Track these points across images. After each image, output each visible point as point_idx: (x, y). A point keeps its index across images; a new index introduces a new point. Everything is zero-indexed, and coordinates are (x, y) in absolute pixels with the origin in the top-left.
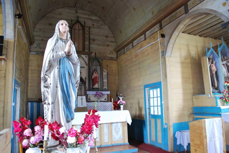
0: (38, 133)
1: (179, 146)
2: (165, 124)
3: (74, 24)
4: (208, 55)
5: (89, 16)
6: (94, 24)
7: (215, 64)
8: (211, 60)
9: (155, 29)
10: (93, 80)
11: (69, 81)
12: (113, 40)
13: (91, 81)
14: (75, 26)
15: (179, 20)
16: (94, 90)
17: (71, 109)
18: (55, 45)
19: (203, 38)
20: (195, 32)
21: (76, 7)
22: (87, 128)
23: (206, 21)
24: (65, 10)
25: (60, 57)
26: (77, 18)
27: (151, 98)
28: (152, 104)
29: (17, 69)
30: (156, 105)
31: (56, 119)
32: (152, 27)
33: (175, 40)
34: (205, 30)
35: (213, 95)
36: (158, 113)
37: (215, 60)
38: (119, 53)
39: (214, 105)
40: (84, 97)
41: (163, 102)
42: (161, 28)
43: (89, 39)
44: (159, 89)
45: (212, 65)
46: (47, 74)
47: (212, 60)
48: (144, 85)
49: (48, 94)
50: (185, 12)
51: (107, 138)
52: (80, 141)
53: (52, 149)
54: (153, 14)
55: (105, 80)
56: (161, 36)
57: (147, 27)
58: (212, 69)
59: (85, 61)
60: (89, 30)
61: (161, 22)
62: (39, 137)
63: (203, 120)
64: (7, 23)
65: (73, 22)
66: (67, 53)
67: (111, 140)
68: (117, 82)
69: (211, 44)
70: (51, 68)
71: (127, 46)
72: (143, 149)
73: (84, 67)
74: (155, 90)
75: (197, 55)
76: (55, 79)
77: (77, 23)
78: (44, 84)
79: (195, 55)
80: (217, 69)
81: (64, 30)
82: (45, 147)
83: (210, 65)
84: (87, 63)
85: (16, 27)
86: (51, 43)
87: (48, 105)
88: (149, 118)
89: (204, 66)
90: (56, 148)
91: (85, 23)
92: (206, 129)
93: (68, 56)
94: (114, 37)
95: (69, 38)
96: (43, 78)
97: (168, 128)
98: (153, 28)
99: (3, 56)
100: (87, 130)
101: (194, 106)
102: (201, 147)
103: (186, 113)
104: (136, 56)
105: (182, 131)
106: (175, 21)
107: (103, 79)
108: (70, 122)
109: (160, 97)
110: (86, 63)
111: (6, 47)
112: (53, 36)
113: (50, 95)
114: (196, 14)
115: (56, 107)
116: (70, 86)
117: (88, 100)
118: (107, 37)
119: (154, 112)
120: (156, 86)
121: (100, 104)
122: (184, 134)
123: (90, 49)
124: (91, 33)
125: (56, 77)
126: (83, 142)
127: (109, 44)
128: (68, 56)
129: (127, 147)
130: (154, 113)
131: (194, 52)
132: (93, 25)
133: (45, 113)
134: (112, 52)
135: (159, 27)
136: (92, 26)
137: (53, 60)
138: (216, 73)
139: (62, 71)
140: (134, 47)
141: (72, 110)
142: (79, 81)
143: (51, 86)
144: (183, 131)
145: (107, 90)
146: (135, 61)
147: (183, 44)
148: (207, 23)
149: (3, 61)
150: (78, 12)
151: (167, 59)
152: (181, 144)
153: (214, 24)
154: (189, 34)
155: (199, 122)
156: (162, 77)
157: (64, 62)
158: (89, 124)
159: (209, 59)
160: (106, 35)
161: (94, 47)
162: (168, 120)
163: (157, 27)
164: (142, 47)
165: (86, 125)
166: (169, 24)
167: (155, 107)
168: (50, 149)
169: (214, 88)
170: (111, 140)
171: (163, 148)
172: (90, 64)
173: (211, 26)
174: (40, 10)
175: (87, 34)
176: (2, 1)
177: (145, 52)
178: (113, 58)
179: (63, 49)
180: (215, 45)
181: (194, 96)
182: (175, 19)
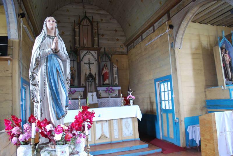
1: (191, 141)
2: (177, 118)
3: (82, 20)
4: (220, 44)
5: (97, 11)
7: (229, 54)
8: (224, 50)
9: (163, 20)
10: (103, 76)
11: (58, 78)
12: (123, 34)
13: (101, 77)
14: (83, 21)
15: (187, 8)
16: (105, 86)
17: (60, 106)
18: (41, 43)
19: (215, 26)
21: (83, 2)
22: (78, 126)
23: (216, 8)
24: (72, 7)
25: (47, 54)
27: (162, 92)
28: (163, 99)
29: (24, 68)
30: (167, 99)
31: (45, 116)
33: (184, 31)
36: (169, 107)
37: (228, 50)
38: (129, 47)
39: (229, 98)
40: (95, 94)
41: (173, 96)
42: (169, 18)
43: (98, 35)
44: (169, 83)
45: (225, 54)
47: (226, 50)
48: (155, 78)
51: (117, 134)
53: (43, 146)
55: (116, 76)
56: (169, 27)
58: (225, 59)
59: (94, 57)
60: (97, 25)
61: (169, 12)
62: (28, 135)
63: (213, 113)
65: (81, 18)
68: (128, 77)
71: (136, 39)
72: (154, 145)
73: (93, 63)
74: (166, 84)
75: (209, 45)
76: (43, 77)
77: (85, 19)
78: (32, 82)
80: (231, 59)
81: (51, 27)
82: (33, 145)
83: (223, 55)
84: (97, 59)
85: (20, 27)
86: (38, 40)
87: (37, 103)
89: (216, 56)
90: (48, 145)
91: (93, 18)
93: (56, 53)
95: (57, 34)
96: (30, 76)
99: (9, 56)
100: (76, 126)
101: (207, 99)
102: (211, 142)
103: (199, 106)
104: (146, 49)
105: (194, 125)
106: (183, 10)
107: (113, 74)
109: (161, 92)
110: (95, 59)
113: (39, 93)
115: (45, 104)
117: (99, 97)
118: (116, 31)
119: (165, 106)
120: (166, 79)
121: (111, 100)
122: (196, 128)
123: (100, 44)
124: (99, 28)
125: (44, 75)
127: (119, 38)
128: (56, 53)
129: (138, 143)
130: (165, 108)
131: (205, 42)
133: (35, 111)
135: (167, 18)
136: (100, 21)
137: (40, 57)
138: (230, 63)
139: (49, 68)
140: (143, 40)
143: (39, 83)
144: (196, 125)
145: (118, 86)
147: (193, 34)
150: (86, 7)
152: (193, 139)
153: (226, 11)
154: (199, 23)
155: (209, 116)
156: (172, 70)
157: (52, 59)
159: (222, 49)
160: (115, 30)
161: (103, 42)
162: (179, 115)
163: (165, 18)
164: (151, 39)
165: (76, 122)
166: (177, 14)
167: (166, 101)
168: (41, 147)
169: (228, 79)
171: (175, 144)
172: (100, 59)
173: (223, 13)
174: (47, 8)
175: (96, 30)
176: (4, 2)
177: (154, 44)
179: (50, 46)
181: (206, 88)
182: (183, 8)
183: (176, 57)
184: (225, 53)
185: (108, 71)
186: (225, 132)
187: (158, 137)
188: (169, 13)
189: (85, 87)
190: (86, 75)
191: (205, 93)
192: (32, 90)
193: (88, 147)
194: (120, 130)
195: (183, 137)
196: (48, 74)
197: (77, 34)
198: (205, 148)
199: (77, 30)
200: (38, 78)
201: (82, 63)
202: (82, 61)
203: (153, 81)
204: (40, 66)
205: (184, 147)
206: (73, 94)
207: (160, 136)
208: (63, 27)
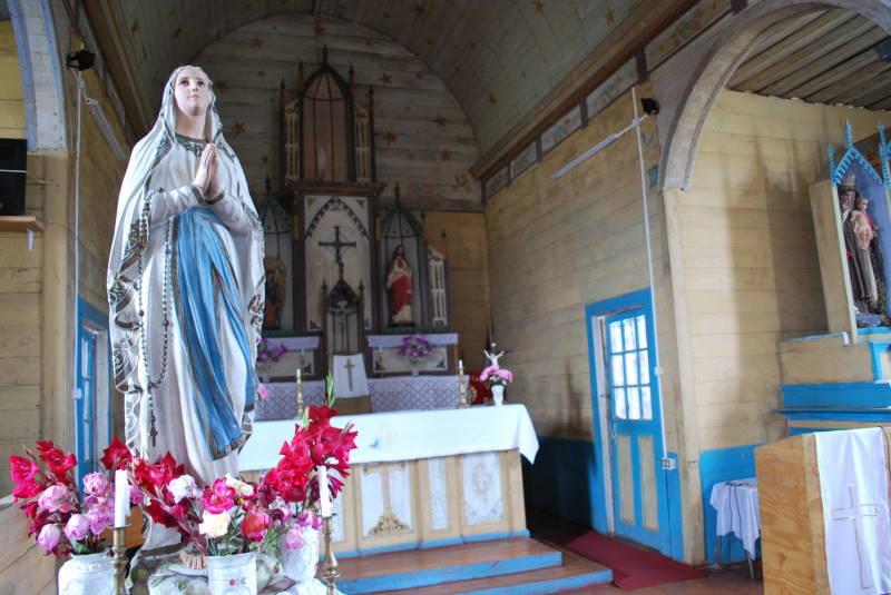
0: (95, 501)
2: (671, 455)
5: (369, 44)
6: (388, 73)
7: (870, 212)
9: (620, 80)
10: (391, 292)
11: (216, 301)
14: (313, 87)
16: (396, 330)
18: (155, 164)
19: (818, 106)
20: (784, 86)
22: (292, 481)
24: (274, 28)
25: (176, 208)
26: (321, 53)
28: (618, 380)
29: (89, 263)
30: (632, 380)
32: (610, 74)
33: (701, 122)
34: (812, 79)
35: (862, 337)
37: (867, 196)
39: (868, 376)
40: (358, 359)
41: (657, 371)
42: (643, 74)
43: (372, 134)
44: (642, 320)
45: (856, 213)
46: (130, 277)
47: (857, 196)
49: (136, 351)
50: (732, 3)
52: (252, 528)
53: (159, 561)
54: (612, 23)
55: (439, 292)
57: (589, 75)
58: (855, 230)
59: (356, 220)
61: (643, 49)
62: (101, 516)
63: (806, 436)
64: (36, 88)
65: (307, 74)
66: (201, 193)
67: (460, 520)
68: (487, 297)
69: (849, 128)
70: (143, 253)
73: (354, 245)
75: (793, 178)
78: (115, 315)
79: (785, 179)
80: (877, 231)
81: (192, 104)
82: (119, 553)
83: (846, 214)
85: (75, 104)
86: (142, 155)
87: (135, 395)
88: (610, 432)
89: (821, 221)
90: (178, 557)
91: (351, 72)
92: (818, 475)
93: (210, 202)
94: (468, 121)
96: (112, 290)
97: (681, 471)
98: (614, 77)
99: (29, 214)
102: (801, 545)
103: (754, 410)
104: (554, 191)
105: (737, 482)
106: (694, 43)
107: (429, 286)
108: (225, 454)
110: (361, 226)
111: (41, 182)
112: (146, 134)
113: (142, 357)
114: (776, 11)
115: (168, 400)
116: (218, 319)
117: (374, 371)
118: (441, 121)
119: (627, 408)
120: (631, 305)
121: (421, 384)
123: (378, 172)
124: (376, 111)
125: (164, 288)
126: (262, 533)
128: (210, 202)
131: (779, 165)
132: (386, 79)
133: (130, 426)
134: (461, 181)
135: (635, 73)
136: (381, 83)
137: (149, 219)
138: (874, 244)
139: (184, 261)
141: (235, 414)
142: (263, 299)
143: (144, 320)
145: (447, 330)
146: (551, 212)
147: (733, 136)
148: (825, 44)
149: (31, 235)
151: (669, 198)
152: (731, 534)
153: (859, 49)
154: (758, 92)
155: (792, 447)
156: (654, 271)
158: (297, 463)
159: (842, 191)
164: (572, 154)
167: (629, 389)
169: (866, 306)
170: (460, 520)
171: (665, 551)
175: (363, 116)
176: (12, 9)
178: (468, 202)
180: (870, 134)
181: (783, 340)
182: (696, 37)
183: (669, 222)
184: (856, 207)
185: (409, 274)
186: (852, 506)
187: (598, 525)
188: (644, 55)
189: (322, 334)
190: (325, 287)
191: (779, 359)
192: (117, 346)
193: (330, 561)
194: (456, 497)
195: (696, 528)
196: (180, 283)
197: (290, 131)
198: (778, 567)
199: (292, 117)
200: (140, 299)
201: (311, 245)
202: (310, 234)
203: (582, 314)
204: (148, 255)
205: (698, 563)
206: (275, 360)
207: (606, 520)
208: (240, 104)
